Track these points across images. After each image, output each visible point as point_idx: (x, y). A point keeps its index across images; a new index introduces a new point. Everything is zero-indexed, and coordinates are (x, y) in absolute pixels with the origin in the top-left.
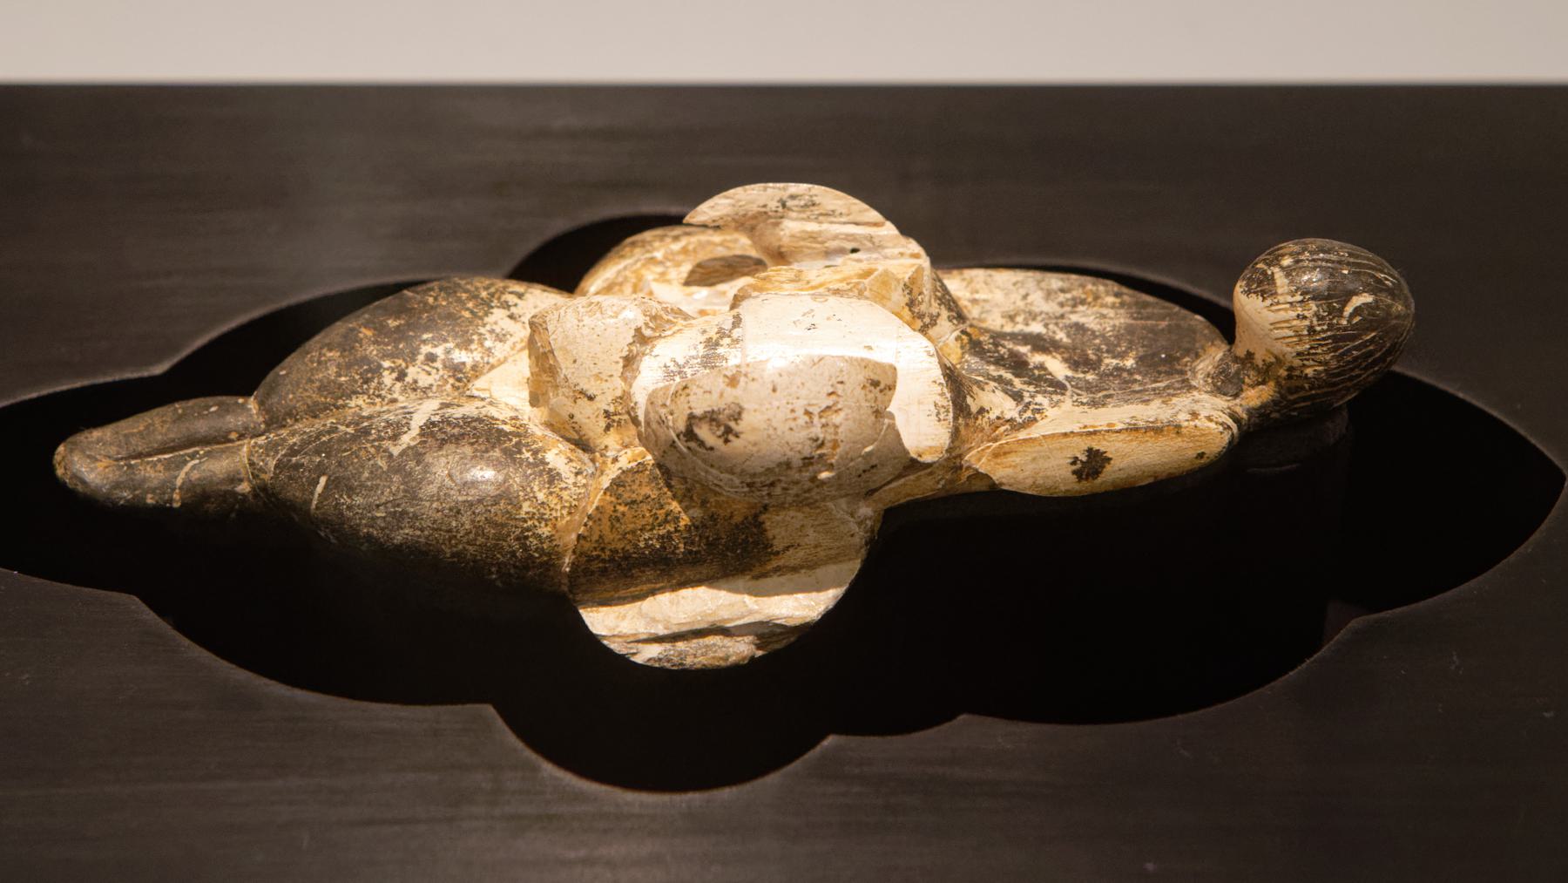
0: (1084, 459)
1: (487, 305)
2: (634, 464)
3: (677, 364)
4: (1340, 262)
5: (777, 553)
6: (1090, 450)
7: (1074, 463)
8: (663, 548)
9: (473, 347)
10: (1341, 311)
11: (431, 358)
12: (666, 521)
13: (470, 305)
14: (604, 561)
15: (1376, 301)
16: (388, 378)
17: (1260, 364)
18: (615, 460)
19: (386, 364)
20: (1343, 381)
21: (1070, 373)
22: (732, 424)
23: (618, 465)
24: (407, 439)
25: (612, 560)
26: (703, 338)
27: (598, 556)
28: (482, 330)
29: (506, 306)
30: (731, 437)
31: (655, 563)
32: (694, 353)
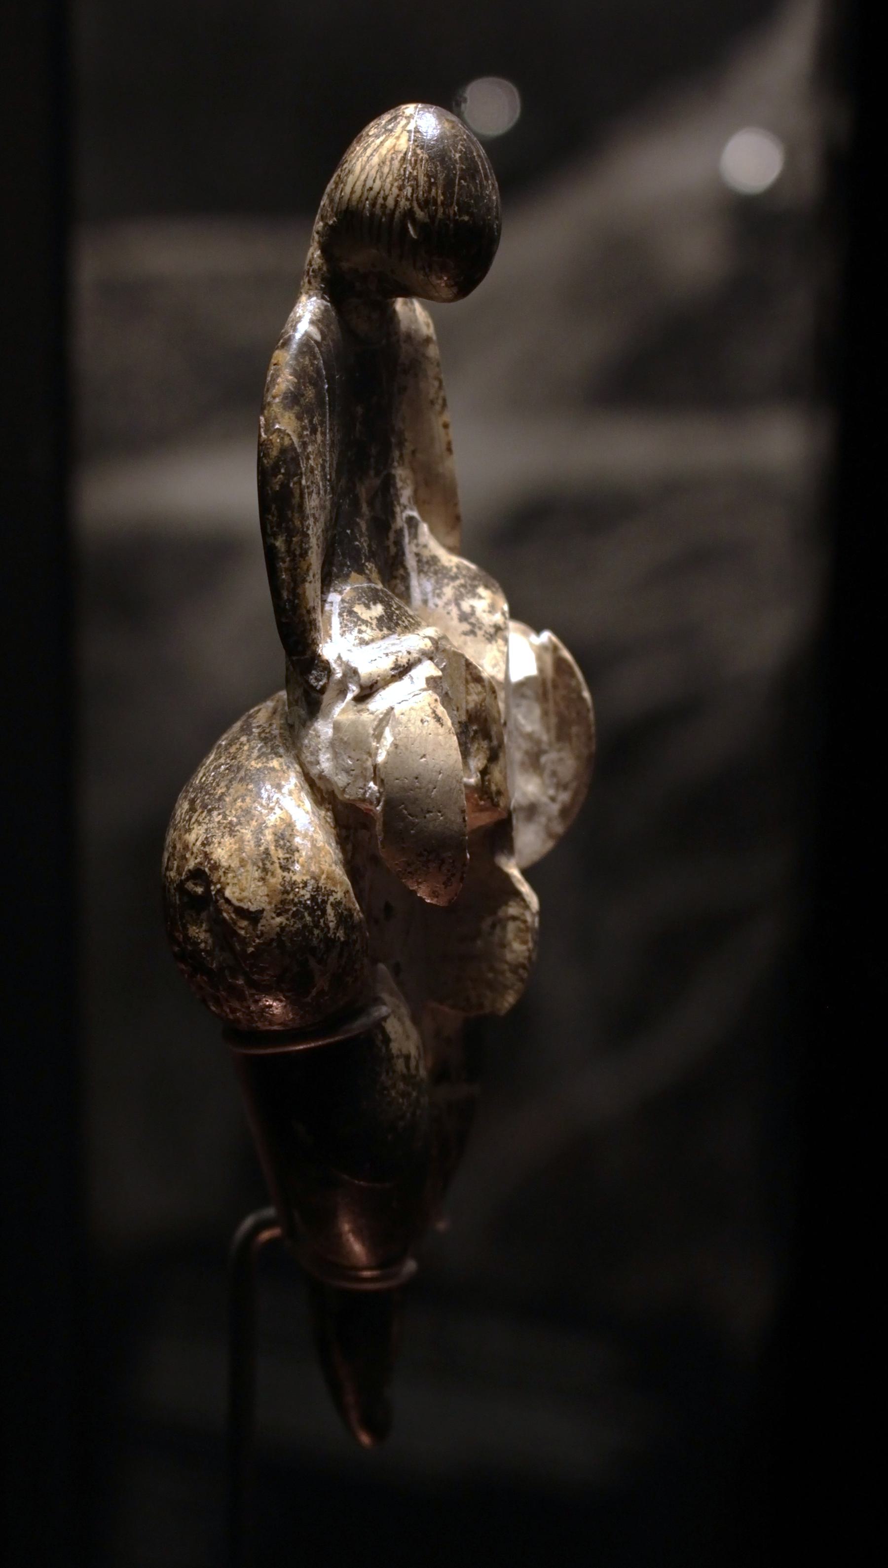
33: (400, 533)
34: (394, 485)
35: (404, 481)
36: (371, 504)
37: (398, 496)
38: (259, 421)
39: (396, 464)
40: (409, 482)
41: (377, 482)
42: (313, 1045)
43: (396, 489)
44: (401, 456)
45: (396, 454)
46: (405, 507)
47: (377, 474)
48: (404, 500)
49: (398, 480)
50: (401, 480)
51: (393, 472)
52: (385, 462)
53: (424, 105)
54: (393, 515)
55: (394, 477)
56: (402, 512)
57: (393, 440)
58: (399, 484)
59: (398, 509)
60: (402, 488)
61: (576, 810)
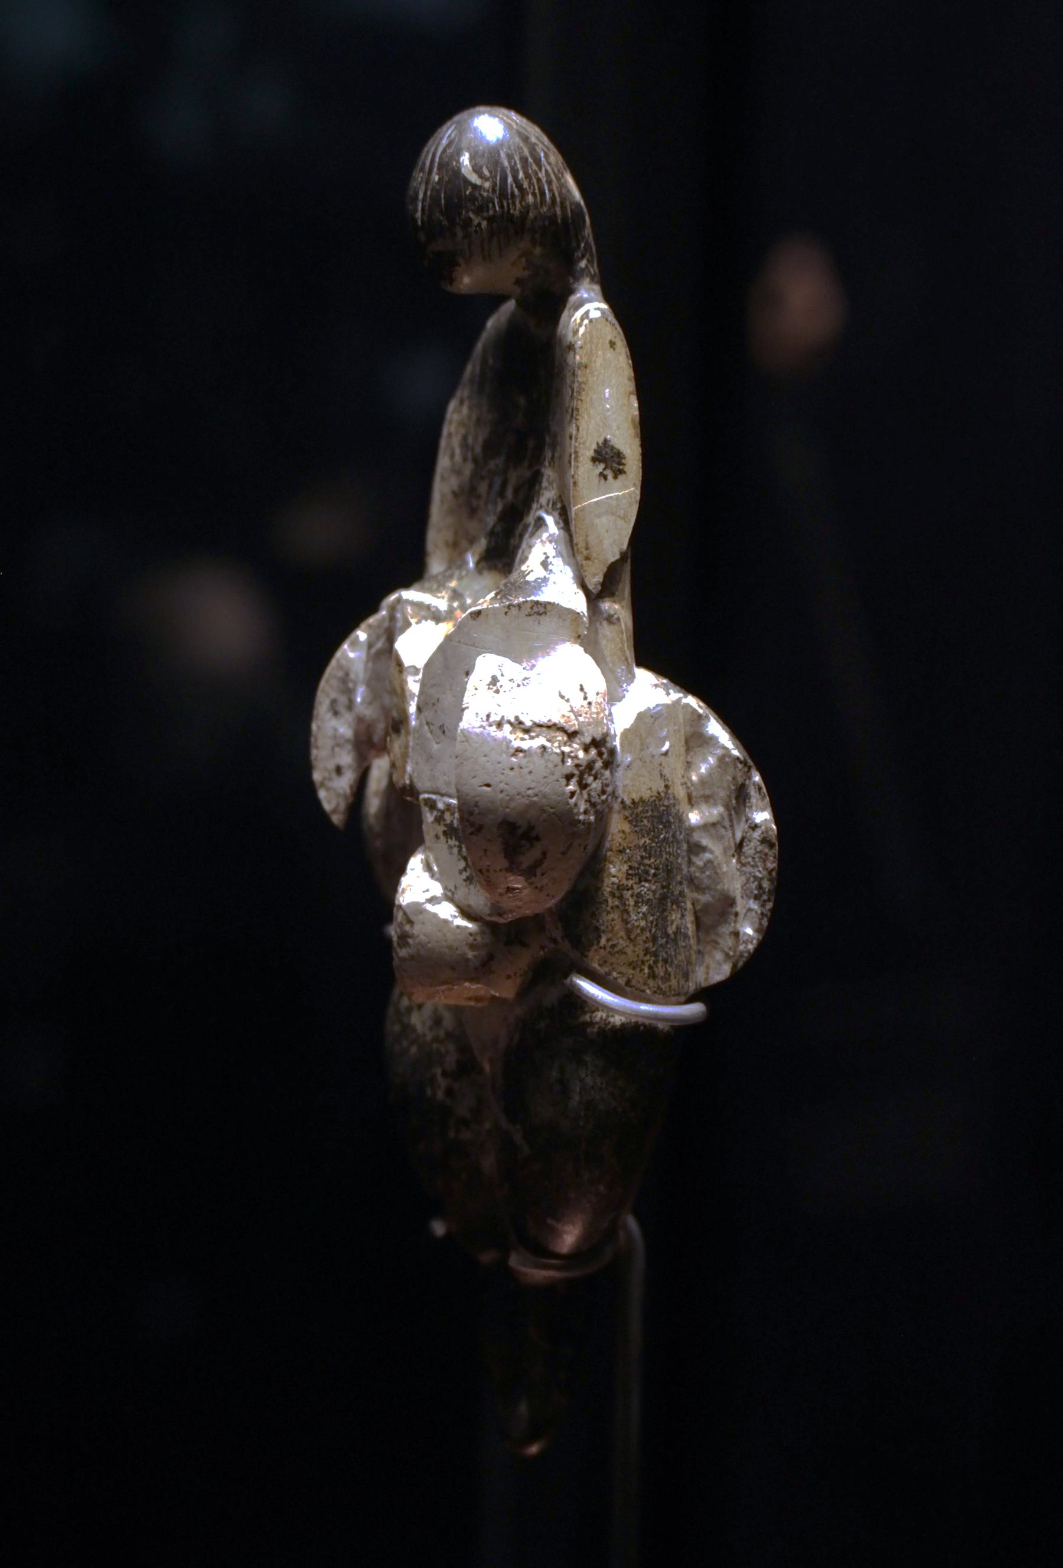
0: (602, 466)
1: (407, 1028)
2: (559, 925)
3: (465, 869)
4: (427, 183)
5: (667, 787)
6: (594, 460)
7: (605, 478)
8: (648, 902)
9: (443, 1050)
10: (475, 187)
11: (449, 1092)
12: (621, 897)
13: (405, 1044)
14: (656, 962)
15: (468, 150)
16: (466, 1135)
17: (527, 273)
18: (554, 941)
19: (452, 1134)
20: (551, 190)
21: (526, 464)
22: (520, 831)
23: (559, 939)
24: (518, 1137)
25: (655, 955)
26: (443, 838)
27: (650, 967)
28: (429, 1038)
29: (409, 1010)
30: (533, 834)
31: (664, 910)
32: (455, 850)
33: (526, 526)
34: (540, 483)
35: (550, 483)
36: (516, 491)
37: (539, 494)
38: (438, 867)
39: (547, 463)
40: (555, 485)
41: (528, 474)
42: (479, 346)
43: (541, 487)
44: (553, 458)
45: (548, 454)
46: (541, 507)
47: (530, 466)
48: (543, 500)
49: (544, 480)
50: (548, 481)
51: (543, 470)
52: (537, 459)
53: (637, 419)
54: (529, 508)
55: (542, 475)
56: (537, 509)
57: (547, 439)
58: (545, 484)
59: (535, 506)
60: (546, 488)
61: (517, 560)
